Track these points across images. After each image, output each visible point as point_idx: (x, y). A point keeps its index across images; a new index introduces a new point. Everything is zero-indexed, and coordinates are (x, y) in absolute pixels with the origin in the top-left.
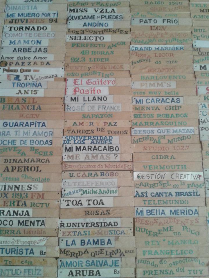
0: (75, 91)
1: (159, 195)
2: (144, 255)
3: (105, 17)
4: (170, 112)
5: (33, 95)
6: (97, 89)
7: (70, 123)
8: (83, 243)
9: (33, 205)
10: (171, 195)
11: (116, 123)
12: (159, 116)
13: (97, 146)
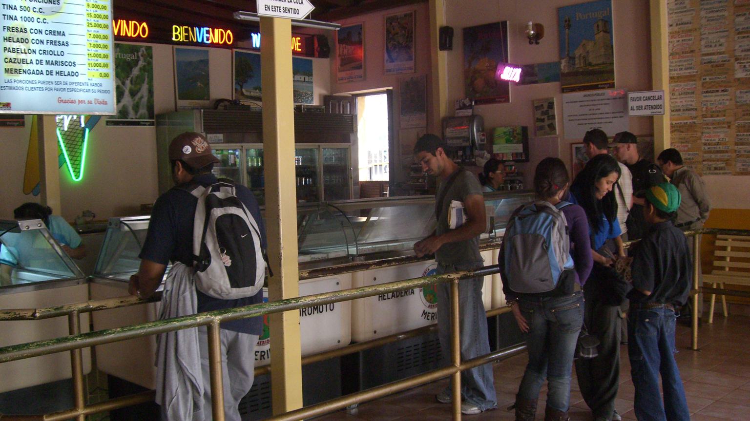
11: (35, 53)
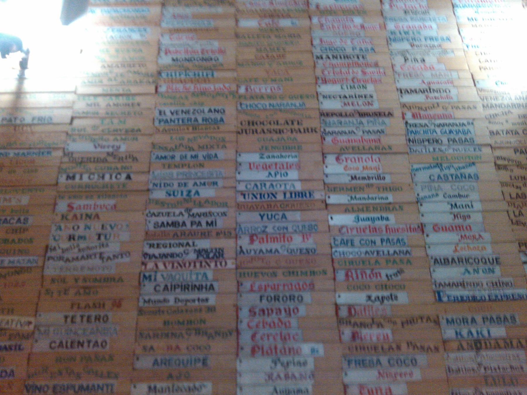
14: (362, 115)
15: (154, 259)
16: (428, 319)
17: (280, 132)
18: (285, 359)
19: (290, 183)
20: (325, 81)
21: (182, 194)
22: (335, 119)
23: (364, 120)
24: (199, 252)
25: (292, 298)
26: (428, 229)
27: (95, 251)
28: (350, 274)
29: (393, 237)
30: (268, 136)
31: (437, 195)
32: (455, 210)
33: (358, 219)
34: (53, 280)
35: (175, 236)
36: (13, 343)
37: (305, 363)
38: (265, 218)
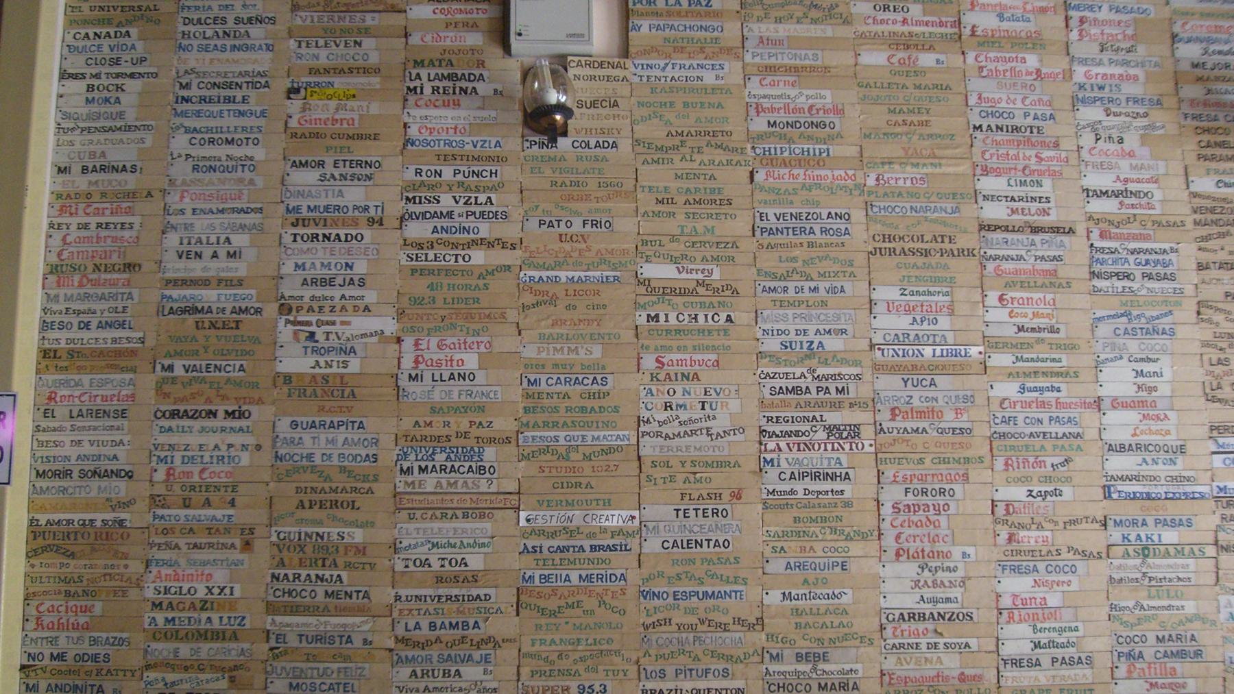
0: (417, 362)
1: (561, 549)
2: (533, 645)
3: (474, 213)
4: (589, 404)
5: (342, 371)
6: (457, 357)
7: (407, 423)
8: (432, 626)
9: (349, 566)
10: (582, 548)
12: (568, 409)
13: (457, 465)
14: (1036, 230)
15: (774, 438)
16: (1094, 520)
17: (927, 253)
18: (933, 564)
19: (940, 333)
20: (986, 171)
21: (802, 348)
22: (998, 236)
23: (1037, 238)
24: (830, 429)
25: (942, 492)
26: (1106, 404)
27: (699, 425)
28: (1010, 462)
29: (1064, 414)
30: (911, 260)
31: (1121, 358)
32: (1140, 380)
33: (1023, 389)
34: (653, 463)
35: (798, 405)
36: (616, 541)
37: (955, 569)
38: (909, 382)
